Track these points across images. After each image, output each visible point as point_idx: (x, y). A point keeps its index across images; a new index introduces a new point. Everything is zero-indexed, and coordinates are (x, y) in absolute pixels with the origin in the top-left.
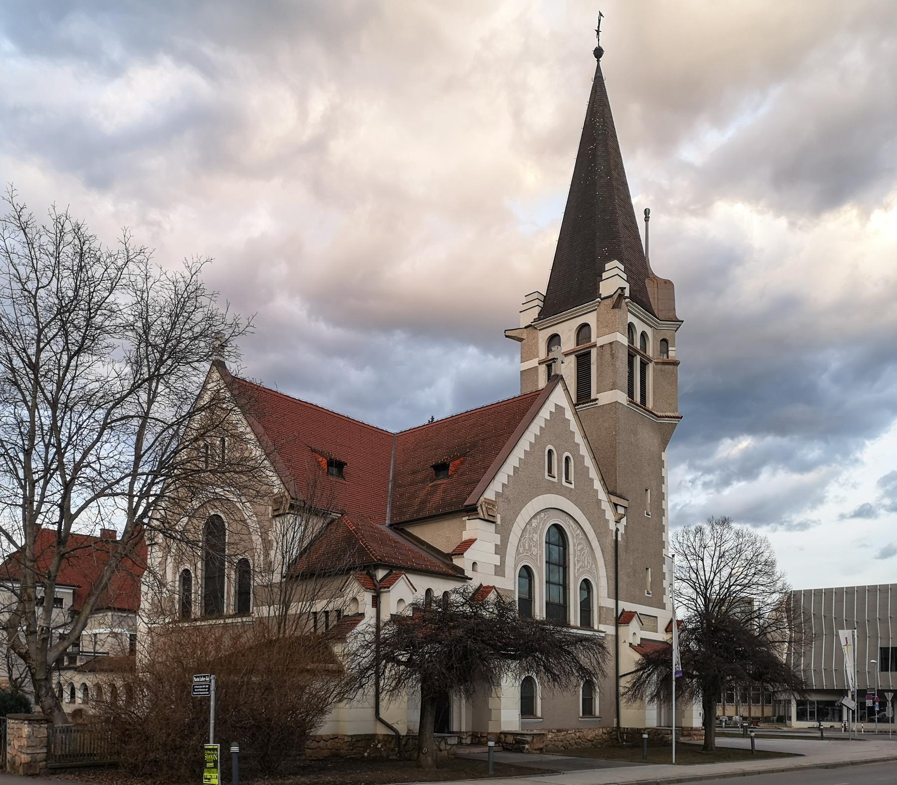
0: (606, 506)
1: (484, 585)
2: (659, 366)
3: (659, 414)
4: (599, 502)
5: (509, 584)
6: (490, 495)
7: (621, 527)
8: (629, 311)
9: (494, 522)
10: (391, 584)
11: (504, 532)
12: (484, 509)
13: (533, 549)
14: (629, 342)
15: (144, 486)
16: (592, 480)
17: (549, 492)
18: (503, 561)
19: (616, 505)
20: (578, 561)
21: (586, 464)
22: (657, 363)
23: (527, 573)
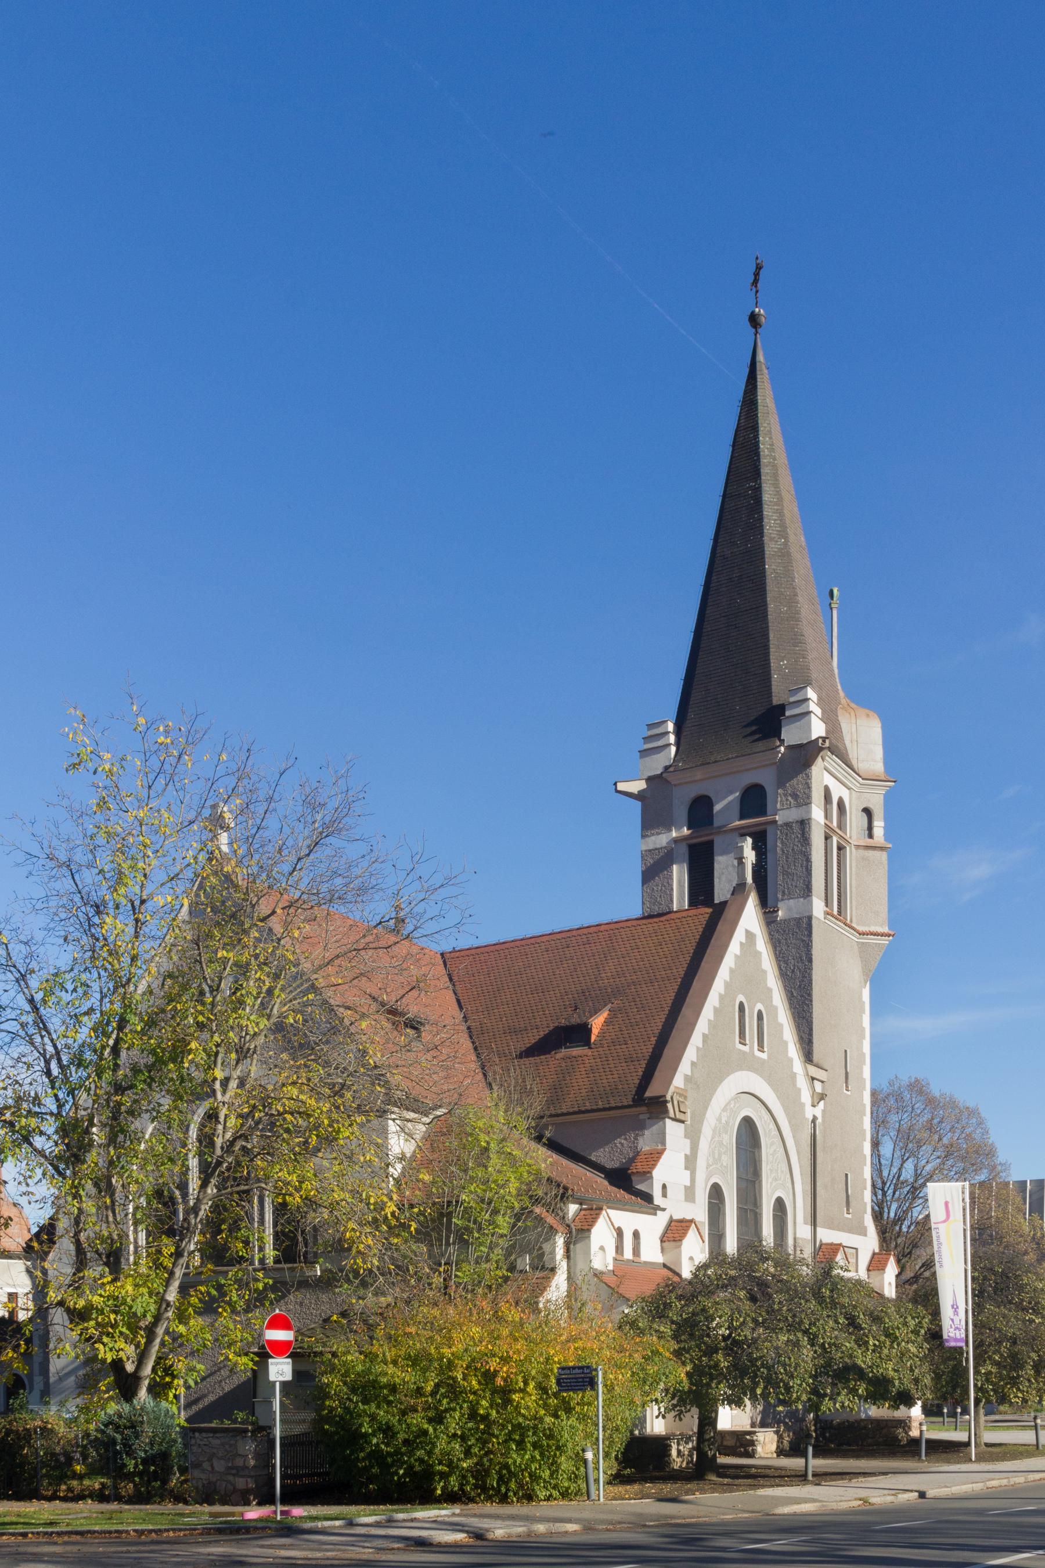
0: (802, 1083)
1: (675, 1218)
2: (861, 852)
3: (861, 929)
4: (793, 1076)
5: (140, 1312)
6: (678, 1081)
7: (818, 1111)
8: (826, 769)
9: (683, 1122)
10: (592, 1226)
11: (693, 1136)
12: (676, 1103)
13: (723, 1157)
14: (826, 817)
15: (875, 1194)
16: (786, 1043)
17: (741, 1068)
18: (693, 1180)
19: (813, 1079)
20: (771, 1171)
21: (774, 1003)
22: (858, 847)
23: (716, 1193)
